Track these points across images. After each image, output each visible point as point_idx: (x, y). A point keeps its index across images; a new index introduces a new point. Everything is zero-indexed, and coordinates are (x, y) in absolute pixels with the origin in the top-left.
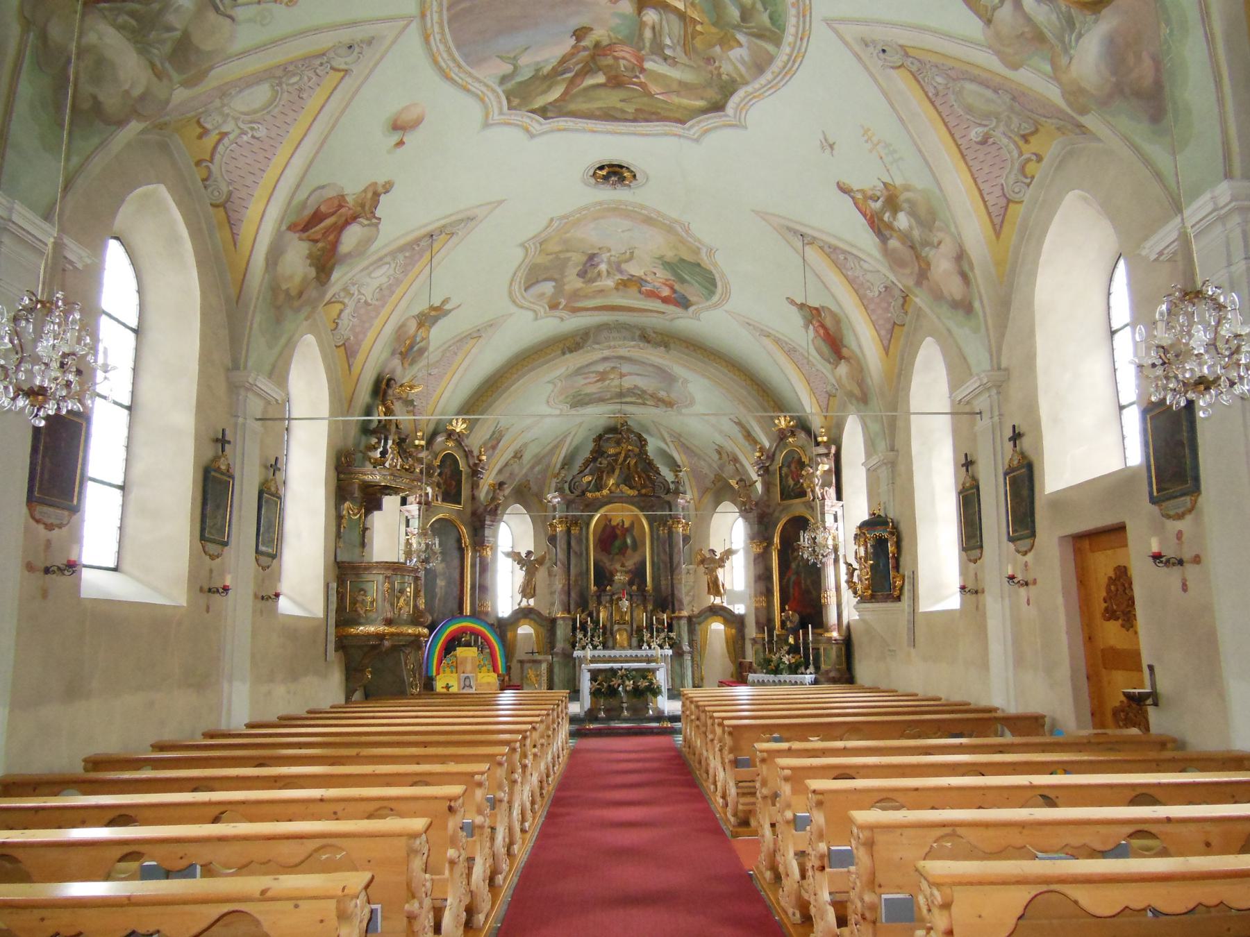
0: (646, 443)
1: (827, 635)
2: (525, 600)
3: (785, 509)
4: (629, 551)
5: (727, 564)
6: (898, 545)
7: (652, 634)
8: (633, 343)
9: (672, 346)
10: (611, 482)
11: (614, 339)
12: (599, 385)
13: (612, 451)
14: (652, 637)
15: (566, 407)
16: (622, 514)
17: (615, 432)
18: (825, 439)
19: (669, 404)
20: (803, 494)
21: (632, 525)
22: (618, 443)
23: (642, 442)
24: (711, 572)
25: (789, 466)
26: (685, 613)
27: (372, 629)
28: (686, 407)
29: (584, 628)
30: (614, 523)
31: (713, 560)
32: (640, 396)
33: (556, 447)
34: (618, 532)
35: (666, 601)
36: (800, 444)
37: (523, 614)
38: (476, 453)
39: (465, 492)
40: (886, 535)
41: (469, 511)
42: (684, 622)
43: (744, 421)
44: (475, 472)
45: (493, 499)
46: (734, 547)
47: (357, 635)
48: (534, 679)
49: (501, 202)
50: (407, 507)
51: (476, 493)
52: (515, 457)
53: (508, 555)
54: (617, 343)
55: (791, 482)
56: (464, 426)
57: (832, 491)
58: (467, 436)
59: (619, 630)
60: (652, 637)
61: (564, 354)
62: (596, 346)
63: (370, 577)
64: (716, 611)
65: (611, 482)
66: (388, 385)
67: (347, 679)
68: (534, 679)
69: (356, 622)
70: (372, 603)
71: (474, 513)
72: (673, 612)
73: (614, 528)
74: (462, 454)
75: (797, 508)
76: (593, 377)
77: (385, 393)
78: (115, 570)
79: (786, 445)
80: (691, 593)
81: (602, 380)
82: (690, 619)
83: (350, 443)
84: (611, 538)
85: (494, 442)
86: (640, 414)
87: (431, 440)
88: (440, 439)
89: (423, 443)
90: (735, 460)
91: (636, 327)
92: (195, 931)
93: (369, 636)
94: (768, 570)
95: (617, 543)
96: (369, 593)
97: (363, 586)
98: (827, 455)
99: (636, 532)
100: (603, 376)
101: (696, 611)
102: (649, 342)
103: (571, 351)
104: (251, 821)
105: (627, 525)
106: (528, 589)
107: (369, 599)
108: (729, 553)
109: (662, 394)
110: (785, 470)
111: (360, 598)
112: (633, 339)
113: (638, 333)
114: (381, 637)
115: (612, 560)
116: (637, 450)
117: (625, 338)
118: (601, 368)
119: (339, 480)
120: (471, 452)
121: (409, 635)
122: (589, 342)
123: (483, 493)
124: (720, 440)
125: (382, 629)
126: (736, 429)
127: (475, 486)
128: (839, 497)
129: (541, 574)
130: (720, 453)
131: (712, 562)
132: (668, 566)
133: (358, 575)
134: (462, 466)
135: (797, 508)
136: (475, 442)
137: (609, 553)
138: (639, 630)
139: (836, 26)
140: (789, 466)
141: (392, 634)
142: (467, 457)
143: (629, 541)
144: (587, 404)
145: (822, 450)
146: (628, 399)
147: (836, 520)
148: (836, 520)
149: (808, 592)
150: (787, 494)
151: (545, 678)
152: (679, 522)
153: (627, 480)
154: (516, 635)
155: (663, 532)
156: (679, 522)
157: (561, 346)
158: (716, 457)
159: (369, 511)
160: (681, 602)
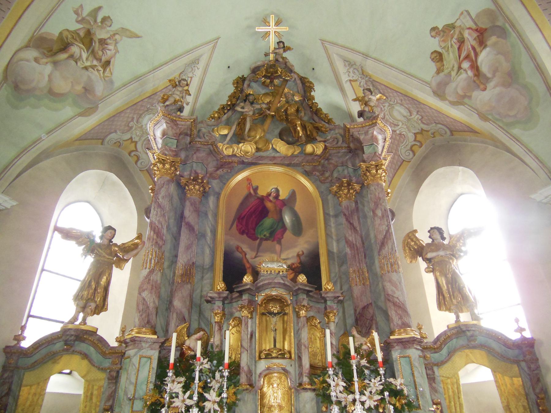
4: (288, 235)
7: (349, 379)
14: (349, 389)
16: (274, 180)
21: (293, 195)
23: (306, 86)
29: (185, 366)
30: (262, 192)
34: (269, 205)
37: (73, 341)
49: (138, 37)
59: (268, 372)
60: (349, 389)
73: (262, 200)
84: (256, 217)
92: (548, 48)
95: (268, 222)
104: (170, 352)
105: (283, 195)
115: (258, 250)
137: (253, 237)
138: (318, 371)
139: (328, 46)
143: (287, 219)
154: (42, 393)
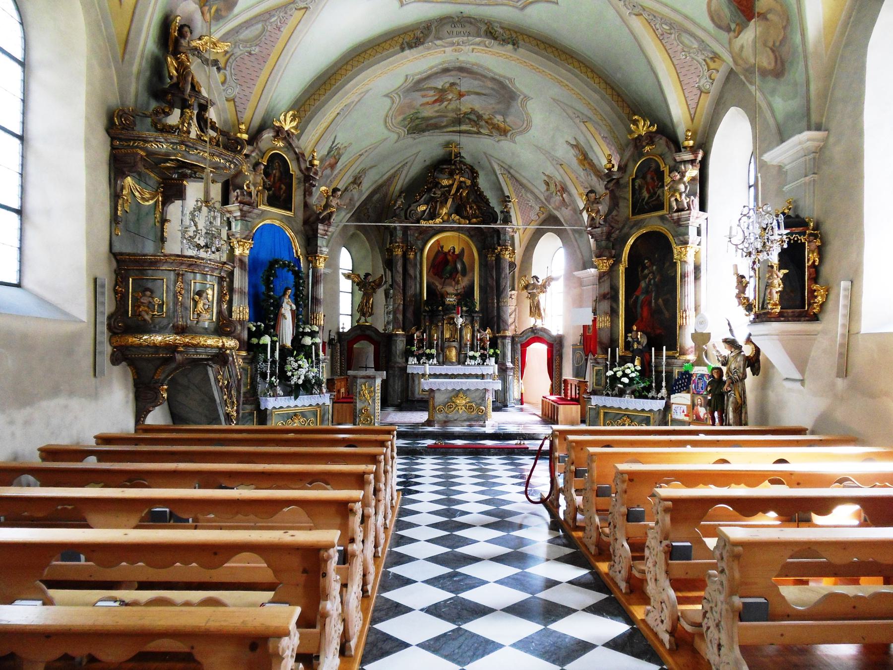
0: (478, 176)
1: (684, 358)
2: (363, 319)
3: (638, 225)
5: (548, 289)
6: (821, 251)
8: (478, 40)
9: (521, 42)
10: (445, 211)
11: (458, 34)
12: (437, 107)
13: (445, 182)
15: (403, 131)
17: (448, 162)
18: (691, 143)
19: (504, 132)
20: (660, 206)
22: (451, 174)
24: (532, 296)
25: (644, 178)
26: (509, 333)
27: (158, 339)
28: (521, 133)
30: (446, 250)
31: (534, 286)
32: (476, 123)
33: (393, 176)
34: (449, 258)
35: (492, 318)
36: (659, 151)
38: (308, 157)
39: (297, 197)
40: (802, 239)
41: (300, 215)
42: (508, 342)
43: (582, 143)
44: (308, 178)
45: (327, 206)
46: (554, 275)
47: (140, 346)
48: (367, 396)
50: (229, 207)
51: (308, 200)
52: (354, 182)
53: (348, 277)
54: (460, 39)
55: (645, 194)
56: (294, 124)
57: (696, 201)
58: (299, 137)
61: (403, 49)
62: (438, 42)
63: (159, 275)
64: (536, 335)
65: (445, 211)
66: (182, 34)
67: (137, 398)
68: (367, 396)
69: (144, 328)
70: (161, 306)
71: (306, 222)
72: (498, 332)
73: (446, 254)
74: (293, 156)
75: (652, 222)
76: (431, 96)
77: (177, 42)
78: (18, 286)
79: (641, 155)
80: (517, 316)
81: (439, 100)
82: (513, 338)
83: (130, 102)
85: (332, 161)
86: (472, 146)
87: (255, 137)
88: (268, 135)
89: (245, 136)
90: (564, 189)
91: (481, 21)
93: (156, 347)
94: (614, 289)
95: (449, 268)
96: (158, 293)
97: (150, 285)
98: (692, 162)
99: (466, 259)
100: (441, 95)
101: (519, 332)
102: (495, 39)
103: (411, 47)
106: (363, 309)
107: (157, 300)
108: (549, 280)
109: (498, 119)
110: (638, 182)
111: (145, 300)
112: (479, 36)
113: (484, 28)
114: (172, 348)
115: (443, 284)
116: (469, 182)
117: (469, 34)
118: (440, 83)
119: (113, 148)
120: (303, 155)
121: (211, 347)
122: (431, 37)
123: (316, 200)
124: (550, 170)
125: (171, 338)
126: (572, 152)
127: (308, 193)
128: (703, 207)
129: (379, 296)
130: (547, 184)
131: (533, 289)
132: (494, 290)
133: (142, 272)
134: (293, 168)
135: (652, 222)
136: (306, 143)
140: (644, 178)
141: (186, 345)
142: (298, 160)
143: (459, 266)
144: (424, 131)
145: (688, 156)
146: (464, 128)
147: (699, 234)
148: (699, 234)
149: (659, 311)
150: (639, 208)
151: (378, 395)
152: (506, 249)
153: (458, 210)
155: (492, 258)
156: (506, 249)
157: (400, 40)
158: (543, 188)
159: (167, 200)
160: (505, 322)
